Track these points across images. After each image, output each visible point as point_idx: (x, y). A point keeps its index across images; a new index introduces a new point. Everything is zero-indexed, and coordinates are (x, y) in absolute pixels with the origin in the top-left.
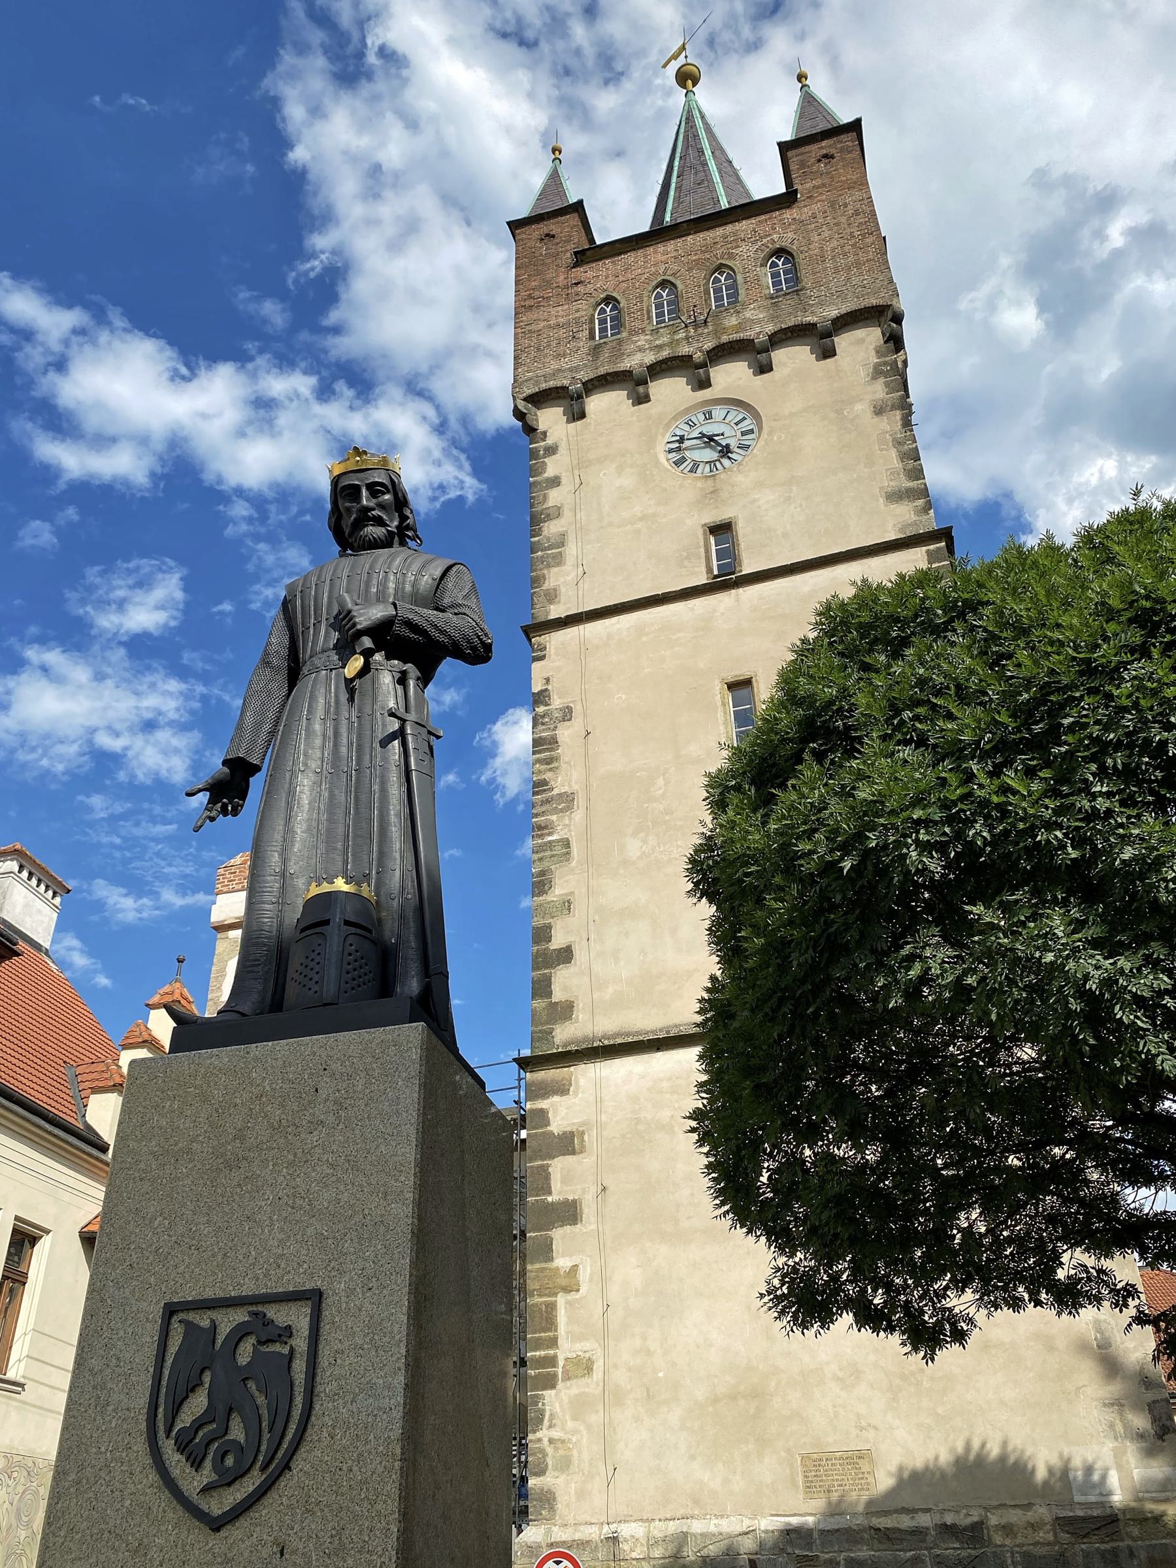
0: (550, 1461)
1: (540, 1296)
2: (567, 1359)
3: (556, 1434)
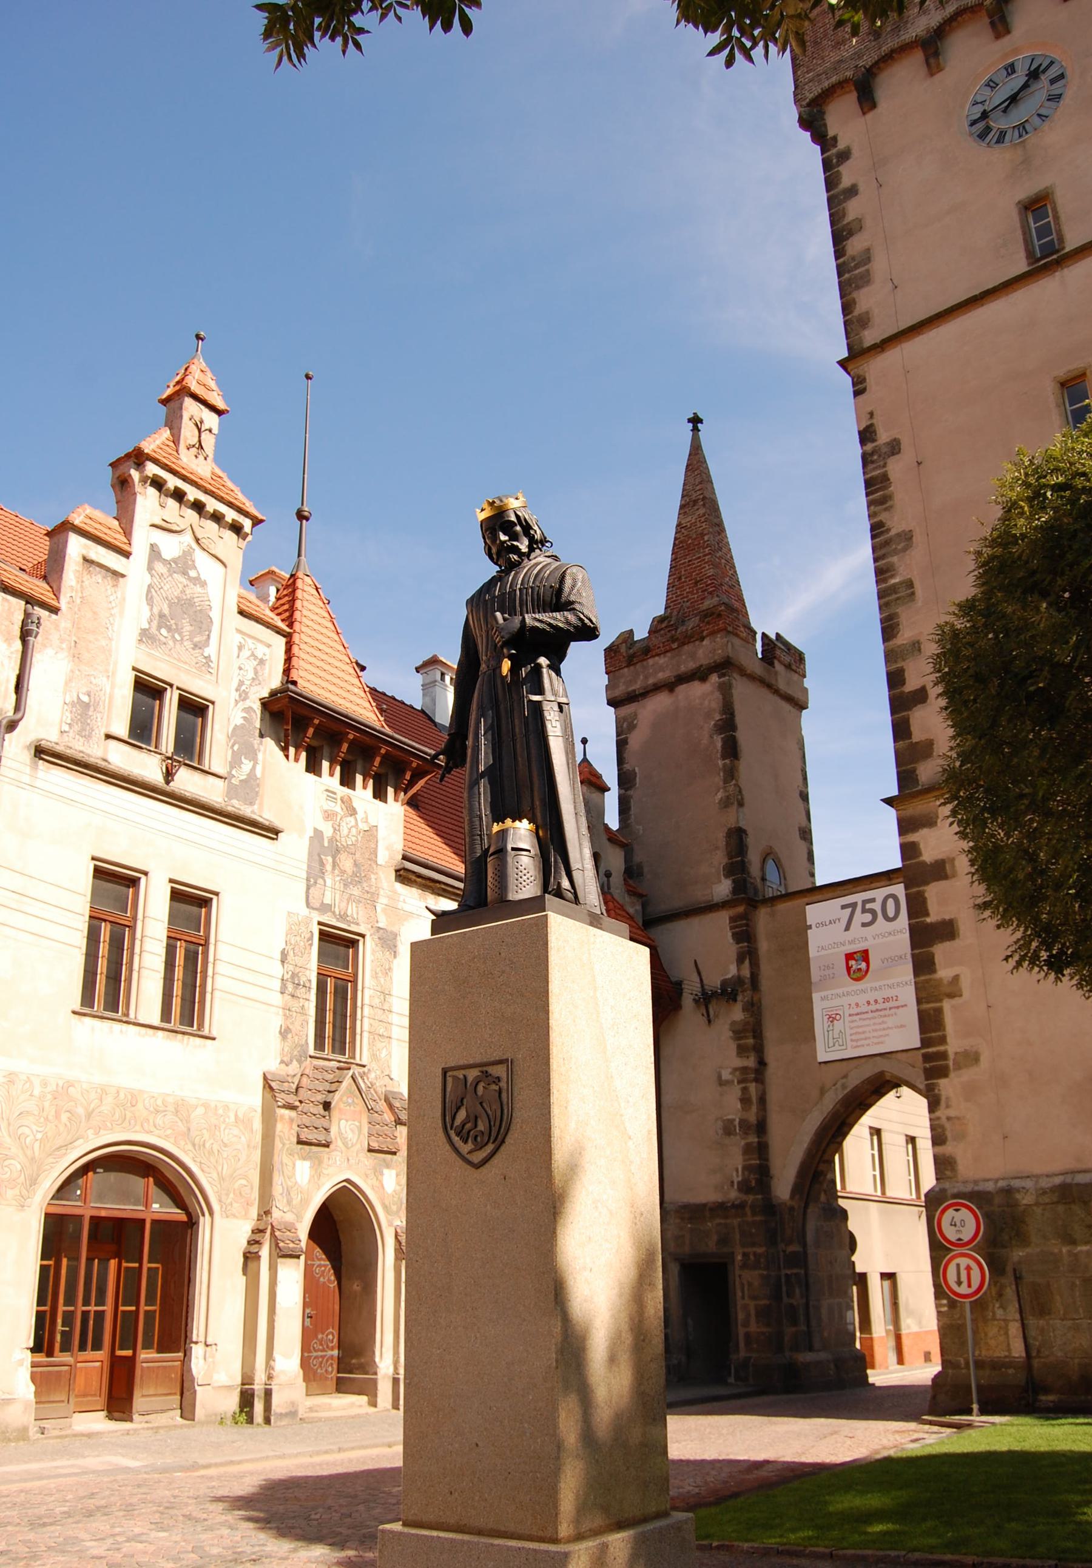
0: (949, 1134)
1: (928, 1002)
2: (956, 1053)
3: (951, 1113)
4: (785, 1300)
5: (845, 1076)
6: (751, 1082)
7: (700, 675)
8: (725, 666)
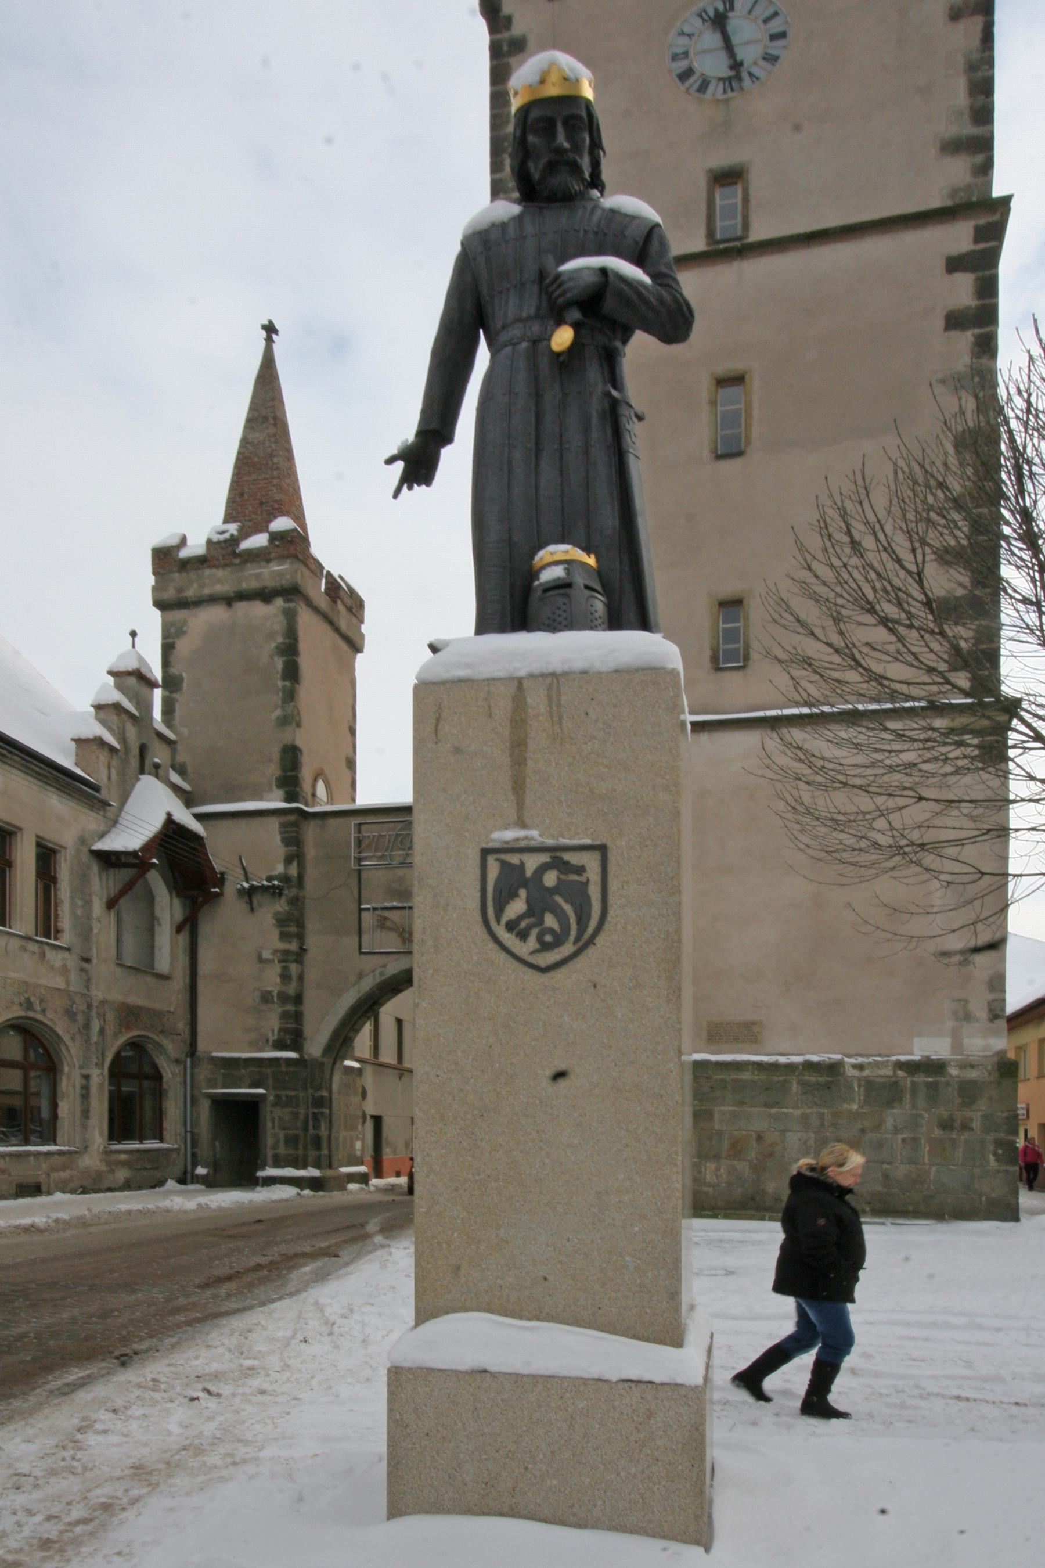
4: (311, 1131)
5: (385, 966)
6: (292, 962)
7: (265, 596)
8: (292, 592)
